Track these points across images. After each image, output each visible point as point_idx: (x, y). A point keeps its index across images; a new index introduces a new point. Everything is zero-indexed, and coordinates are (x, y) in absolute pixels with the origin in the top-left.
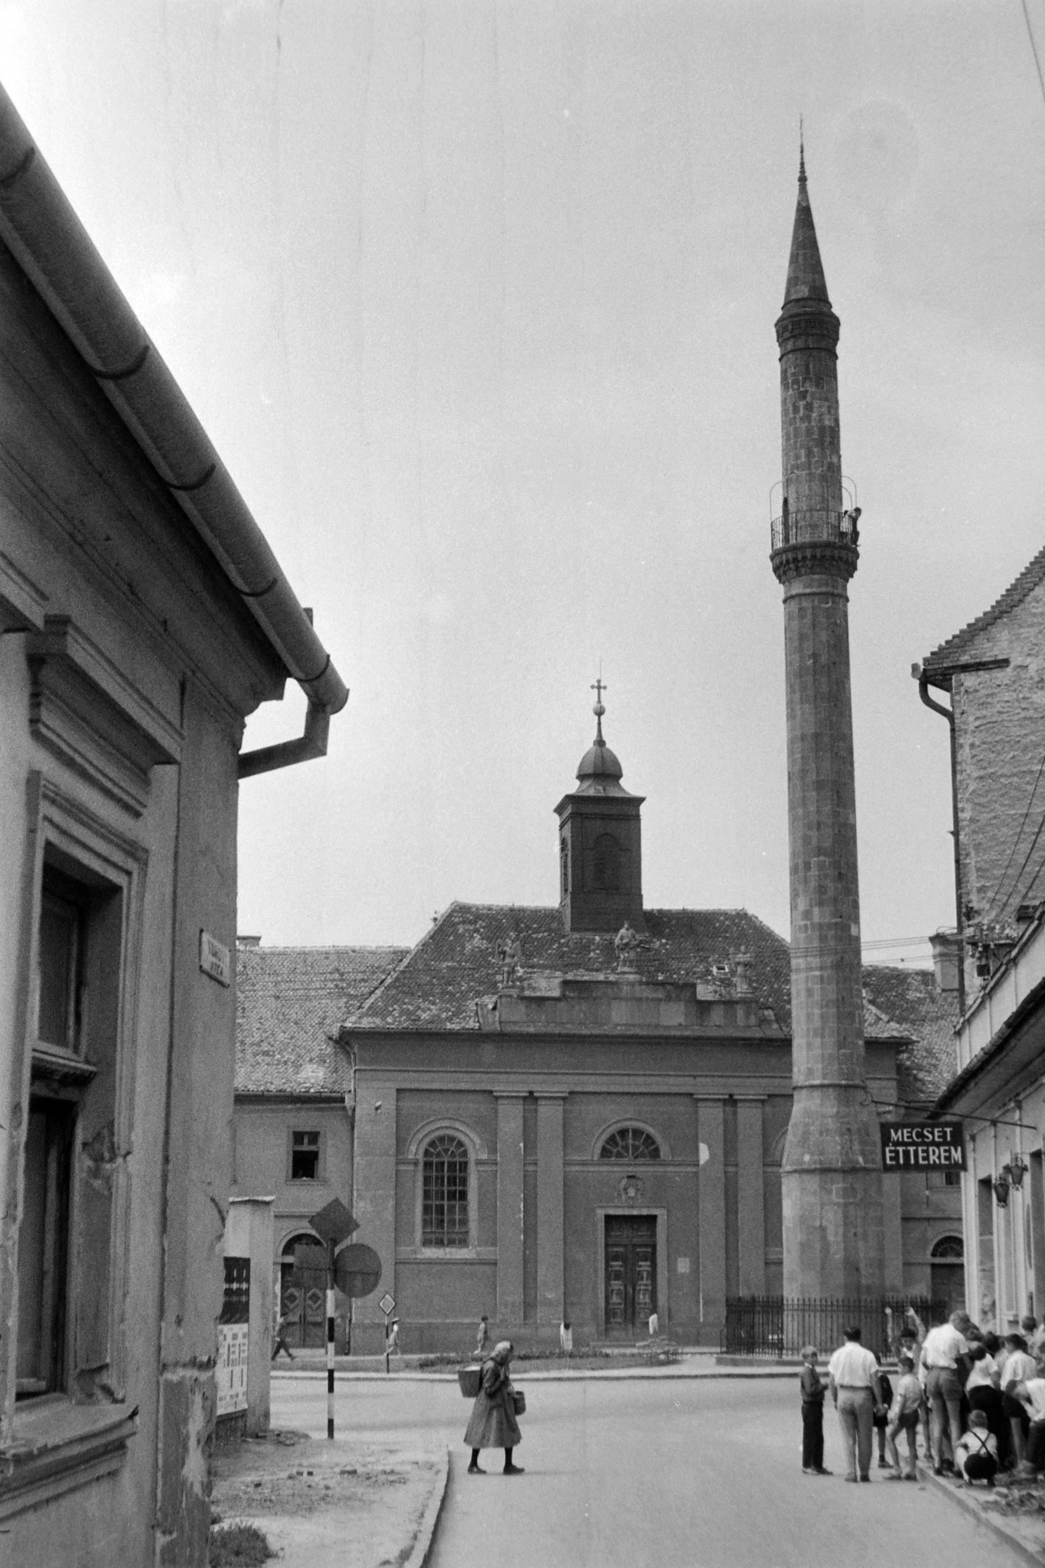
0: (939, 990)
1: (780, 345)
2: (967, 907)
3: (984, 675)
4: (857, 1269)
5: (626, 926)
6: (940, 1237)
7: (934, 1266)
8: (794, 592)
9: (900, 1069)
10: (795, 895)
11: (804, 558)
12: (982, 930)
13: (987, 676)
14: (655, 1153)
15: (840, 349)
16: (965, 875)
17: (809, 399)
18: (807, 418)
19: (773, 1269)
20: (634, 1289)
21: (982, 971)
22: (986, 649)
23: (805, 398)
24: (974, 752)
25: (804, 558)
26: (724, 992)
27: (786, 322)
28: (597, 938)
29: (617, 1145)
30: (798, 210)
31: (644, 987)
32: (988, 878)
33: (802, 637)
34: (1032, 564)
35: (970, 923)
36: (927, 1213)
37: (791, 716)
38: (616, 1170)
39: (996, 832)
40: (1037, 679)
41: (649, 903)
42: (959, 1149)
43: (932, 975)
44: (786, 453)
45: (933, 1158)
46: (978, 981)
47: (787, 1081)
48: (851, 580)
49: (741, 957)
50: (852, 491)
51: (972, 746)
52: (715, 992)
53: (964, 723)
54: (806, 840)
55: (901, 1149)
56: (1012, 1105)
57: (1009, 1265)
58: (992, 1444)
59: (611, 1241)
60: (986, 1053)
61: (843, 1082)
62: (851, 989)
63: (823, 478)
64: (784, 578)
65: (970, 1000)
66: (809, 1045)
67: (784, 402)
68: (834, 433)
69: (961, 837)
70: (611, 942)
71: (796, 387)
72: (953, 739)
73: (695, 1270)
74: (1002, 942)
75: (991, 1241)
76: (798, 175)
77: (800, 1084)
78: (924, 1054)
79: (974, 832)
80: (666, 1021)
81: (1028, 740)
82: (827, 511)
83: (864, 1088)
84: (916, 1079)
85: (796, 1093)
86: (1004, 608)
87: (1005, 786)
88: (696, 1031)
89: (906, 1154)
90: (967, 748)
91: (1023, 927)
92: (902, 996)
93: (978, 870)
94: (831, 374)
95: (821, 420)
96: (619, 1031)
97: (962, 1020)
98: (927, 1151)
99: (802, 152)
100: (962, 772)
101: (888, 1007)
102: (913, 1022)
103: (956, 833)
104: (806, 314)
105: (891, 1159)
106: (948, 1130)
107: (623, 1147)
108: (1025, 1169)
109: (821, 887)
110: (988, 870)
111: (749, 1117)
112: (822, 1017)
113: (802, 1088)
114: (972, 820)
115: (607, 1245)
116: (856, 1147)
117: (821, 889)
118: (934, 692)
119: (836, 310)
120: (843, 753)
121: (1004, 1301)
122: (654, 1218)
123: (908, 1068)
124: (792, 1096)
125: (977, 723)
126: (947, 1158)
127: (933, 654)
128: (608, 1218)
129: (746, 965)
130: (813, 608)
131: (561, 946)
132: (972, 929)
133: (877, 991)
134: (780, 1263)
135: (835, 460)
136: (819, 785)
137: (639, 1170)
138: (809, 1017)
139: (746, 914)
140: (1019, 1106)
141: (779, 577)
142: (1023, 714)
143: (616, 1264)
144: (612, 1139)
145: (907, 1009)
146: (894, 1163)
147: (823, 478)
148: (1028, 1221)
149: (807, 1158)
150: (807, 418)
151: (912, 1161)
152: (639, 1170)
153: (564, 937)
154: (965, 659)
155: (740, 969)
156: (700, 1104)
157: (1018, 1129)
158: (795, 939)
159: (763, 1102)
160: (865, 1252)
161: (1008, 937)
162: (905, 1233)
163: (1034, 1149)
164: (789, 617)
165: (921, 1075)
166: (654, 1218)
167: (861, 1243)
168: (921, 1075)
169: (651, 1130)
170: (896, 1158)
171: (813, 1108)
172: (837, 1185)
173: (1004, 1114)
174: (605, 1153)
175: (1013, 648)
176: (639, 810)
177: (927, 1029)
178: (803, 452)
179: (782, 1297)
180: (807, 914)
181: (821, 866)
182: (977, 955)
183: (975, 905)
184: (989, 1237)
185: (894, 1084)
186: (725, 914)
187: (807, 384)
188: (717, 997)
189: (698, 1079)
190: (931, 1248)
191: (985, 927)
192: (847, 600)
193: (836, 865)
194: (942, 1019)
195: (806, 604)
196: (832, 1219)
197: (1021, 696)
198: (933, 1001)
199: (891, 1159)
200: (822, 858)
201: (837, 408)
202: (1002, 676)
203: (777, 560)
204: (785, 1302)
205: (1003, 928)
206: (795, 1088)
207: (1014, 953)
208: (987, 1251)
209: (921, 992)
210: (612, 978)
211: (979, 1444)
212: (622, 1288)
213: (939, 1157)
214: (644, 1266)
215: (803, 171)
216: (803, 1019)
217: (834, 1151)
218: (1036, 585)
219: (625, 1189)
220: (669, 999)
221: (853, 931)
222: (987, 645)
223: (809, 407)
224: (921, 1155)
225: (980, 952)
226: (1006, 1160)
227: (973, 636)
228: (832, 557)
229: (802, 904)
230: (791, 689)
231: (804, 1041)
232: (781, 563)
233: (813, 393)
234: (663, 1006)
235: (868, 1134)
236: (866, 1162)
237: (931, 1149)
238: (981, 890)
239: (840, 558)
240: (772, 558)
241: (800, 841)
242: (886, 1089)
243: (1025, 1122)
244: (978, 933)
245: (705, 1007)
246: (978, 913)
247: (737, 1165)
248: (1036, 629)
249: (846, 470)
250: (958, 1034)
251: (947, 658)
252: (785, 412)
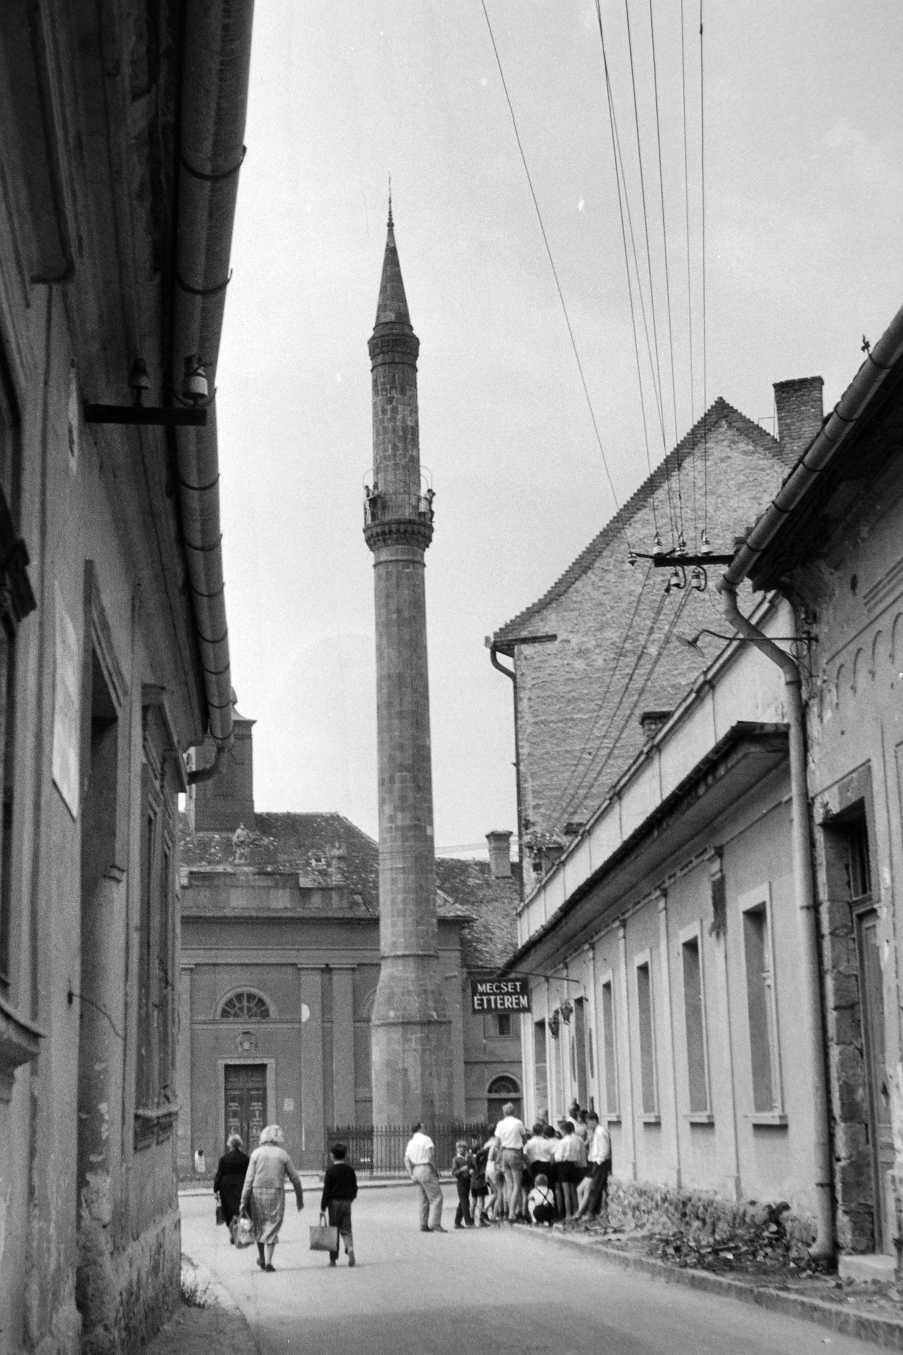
0: (493, 878)
1: (372, 359)
2: (525, 819)
3: (538, 646)
4: (432, 1102)
5: (242, 826)
6: (494, 1078)
7: (490, 1101)
8: (382, 559)
9: (464, 942)
10: (382, 802)
11: (391, 532)
12: (537, 837)
13: (540, 647)
14: (265, 1014)
15: (419, 363)
16: (524, 796)
17: (394, 403)
18: (393, 419)
19: (362, 1106)
20: (248, 1124)
21: (537, 867)
22: (541, 627)
23: (391, 402)
24: (531, 704)
25: (391, 532)
26: (321, 881)
27: (375, 341)
28: (217, 836)
29: (234, 1007)
30: (387, 250)
31: (256, 877)
32: (540, 798)
33: (388, 596)
34: (573, 564)
35: (528, 831)
36: (486, 1058)
37: (380, 658)
38: (233, 1028)
39: (547, 763)
40: (577, 650)
41: (260, 807)
42: (526, 997)
43: (488, 865)
44: (376, 445)
45: (507, 1004)
46: (533, 875)
47: (377, 952)
48: (427, 550)
49: (336, 852)
50: (429, 479)
51: (529, 699)
52: (314, 880)
53: (524, 682)
54: (391, 758)
55: (485, 998)
56: (562, 965)
57: (559, 1082)
58: (550, 1198)
59: (229, 1087)
60: (545, 929)
61: (420, 953)
62: (427, 878)
63: (405, 467)
64: (374, 547)
65: (528, 890)
66: (394, 925)
67: (375, 405)
68: (415, 430)
69: (522, 768)
70: (229, 840)
71: (384, 393)
72: (516, 693)
73: (298, 1106)
74: (551, 846)
75: (545, 1068)
76: (387, 221)
77: (386, 955)
78: (482, 929)
79: (531, 764)
80: (274, 905)
81: (569, 696)
82: (409, 494)
83: (437, 957)
84: (476, 950)
85: (383, 963)
86: (553, 596)
87: (554, 729)
88: (300, 912)
89: (489, 1001)
90: (525, 701)
91: (570, 838)
92: (464, 882)
93: (534, 792)
94: (413, 384)
95: (404, 421)
96: (237, 913)
97: (522, 905)
98: (503, 999)
99: (390, 202)
100: (523, 717)
101: (453, 892)
102: (473, 904)
103: (517, 764)
104: (393, 335)
105: (479, 1005)
106: (518, 984)
107: (239, 1009)
108: (571, 1011)
109: (403, 797)
110: (540, 792)
111: (342, 983)
112: (405, 900)
113: (388, 957)
114: (529, 755)
115: (226, 1089)
116: (431, 1004)
117: (403, 798)
118: (501, 658)
119: (416, 332)
120: (420, 591)
121: (555, 1108)
122: (263, 1067)
123: (469, 941)
124: (378, 965)
125: (534, 682)
126: (518, 1004)
127: (501, 629)
128: (227, 1067)
129: (340, 858)
130: (399, 572)
131: (187, 843)
132: (529, 836)
133: (444, 880)
134: (370, 1100)
135: (415, 453)
136: (401, 715)
137: (251, 1027)
138: (394, 902)
139: (338, 817)
140: (566, 966)
141: (370, 546)
142: (567, 676)
143: (234, 1105)
144: (230, 1003)
145: (468, 893)
146: (480, 1008)
147: (405, 467)
148: (573, 1049)
149: (392, 1014)
150: (393, 419)
151: (493, 1006)
152: (251, 1027)
153: (189, 835)
154: (524, 634)
155: (334, 862)
156: (303, 972)
157: (565, 982)
158: (383, 841)
159: (353, 970)
160: (438, 1088)
161: (555, 842)
162: (467, 1075)
163: (577, 996)
164: (378, 578)
165: (480, 946)
166: (263, 1067)
167: (435, 1081)
168: (480, 946)
169: (261, 994)
170: (481, 1004)
171: (396, 974)
172: (416, 1035)
173: (555, 972)
174: (225, 1013)
175: (560, 627)
176: (250, 730)
177: (484, 909)
178: (390, 446)
179: (372, 1128)
180: (392, 819)
181: (403, 780)
182: (533, 855)
183: (531, 818)
184: (542, 1065)
185: (458, 954)
186: (321, 816)
187: (394, 392)
188: (315, 885)
189: (301, 952)
190: (487, 1087)
191: (539, 835)
192: (424, 565)
193: (415, 779)
194: (497, 901)
195: (391, 568)
196: (412, 1062)
197: (565, 662)
198: (489, 886)
199: (479, 1005)
200: (404, 773)
201: (416, 412)
202: (550, 647)
203: (369, 532)
204: (375, 1130)
205: (552, 835)
206: (383, 958)
207: (563, 858)
208: (541, 1074)
209: (479, 879)
210: (229, 869)
211: (542, 1197)
212: (239, 1124)
213: (512, 1004)
214: (256, 1106)
215: (390, 219)
216: (389, 903)
217: (414, 1007)
218: (577, 579)
219: (241, 1044)
220: (276, 886)
221: (429, 832)
222: (541, 624)
223: (395, 410)
224: (499, 1002)
225: (535, 854)
226: (557, 1006)
227: (531, 617)
228: (413, 532)
229: (388, 810)
230: (380, 635)
231: (389, 922)
232: (372, 535)
233: (398, 399)
234: (272, 891)
235: (441, 995)
236: (438, 1016)
237: (506, 998)
238: (536, 807)
239: (419, 533)
240: (365, 531)
241: (386, 760)
242: (452, 959)
243: (570, 978)
244: (533, 838)
245: (306, 893)
246: (534, 824)
247: (332, 1022)
248: (576, 613)
249: (423, 461)
250: (519, 915)
251: (511, 632)
252: (375, 414)
